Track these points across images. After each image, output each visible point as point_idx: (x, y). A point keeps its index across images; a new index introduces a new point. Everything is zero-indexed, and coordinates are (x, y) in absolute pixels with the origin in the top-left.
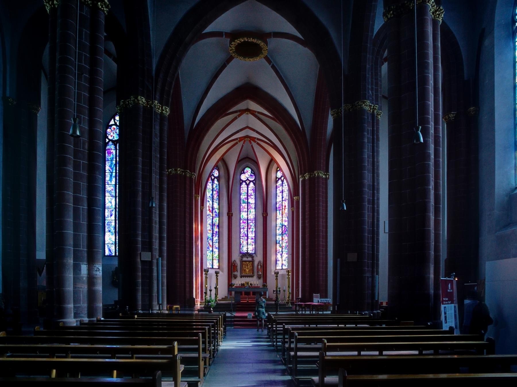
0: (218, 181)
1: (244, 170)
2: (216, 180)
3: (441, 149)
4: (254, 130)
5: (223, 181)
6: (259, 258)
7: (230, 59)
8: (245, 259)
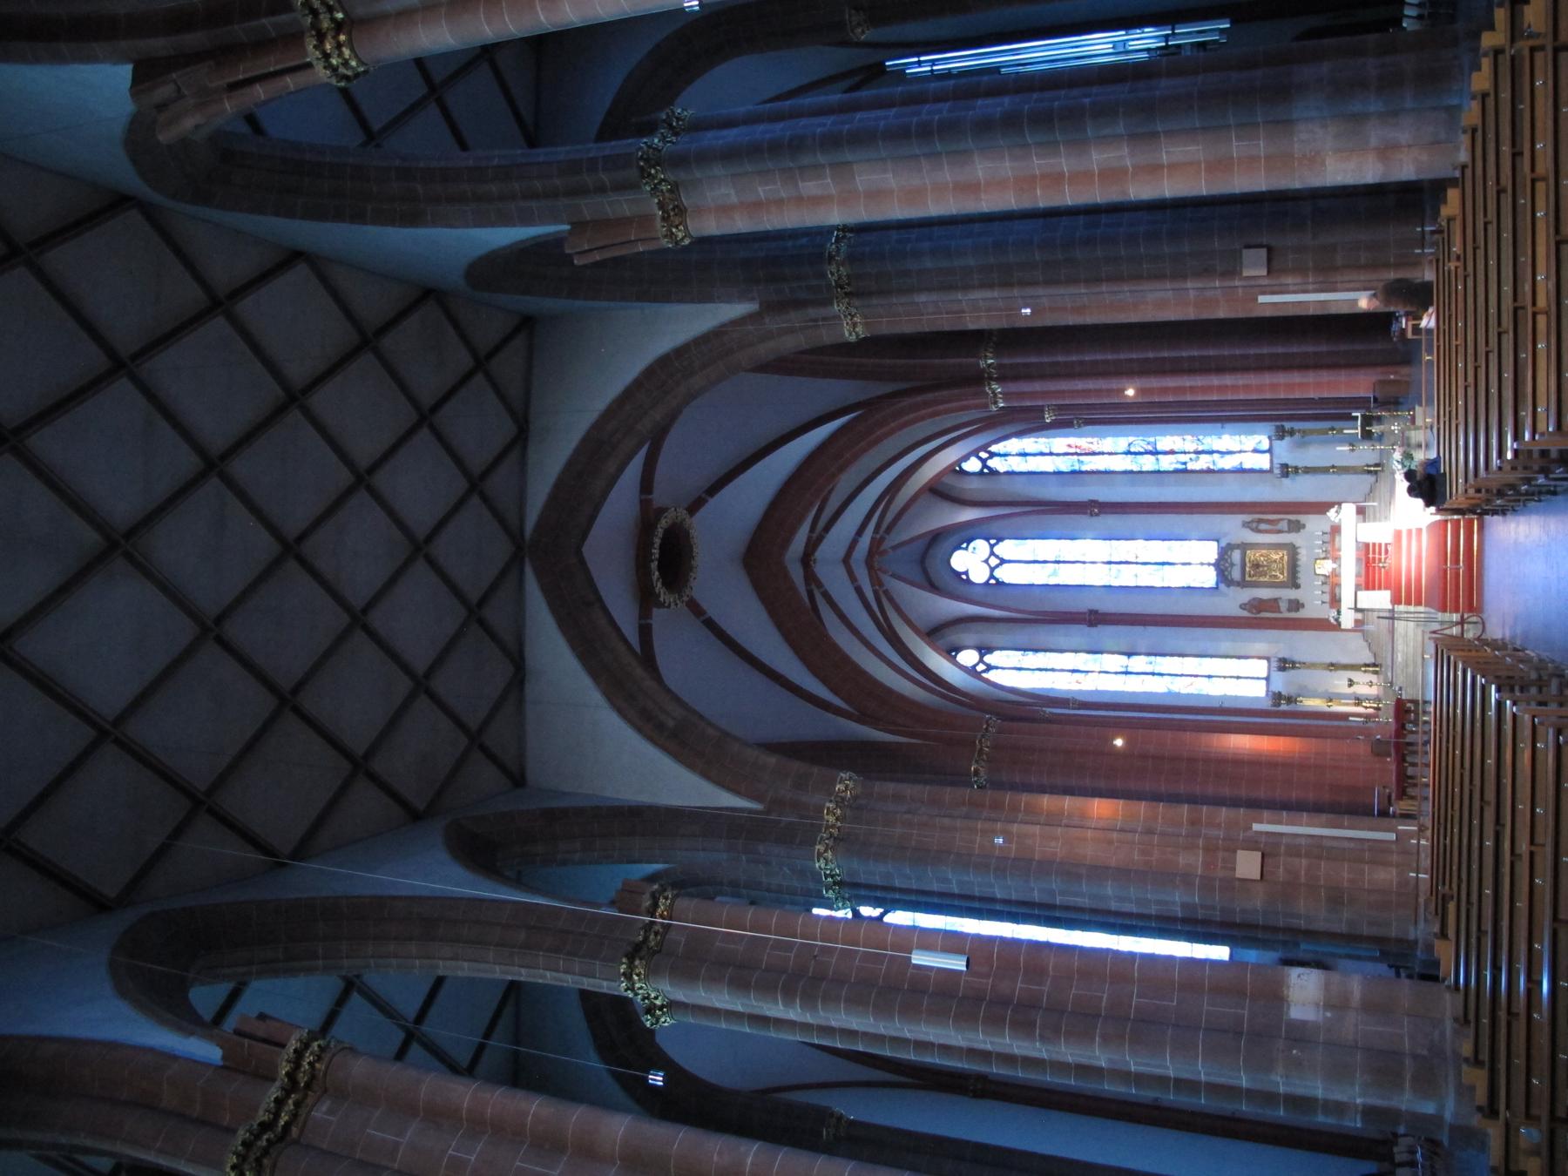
0: (990, 650)
1: (958, 574)
2: (987, 659)
3: (985, 78)
4: (854, 543)
5: (989, 636)
6: (1233, 527)
7: (695, 608)
8: (1236, 574)
